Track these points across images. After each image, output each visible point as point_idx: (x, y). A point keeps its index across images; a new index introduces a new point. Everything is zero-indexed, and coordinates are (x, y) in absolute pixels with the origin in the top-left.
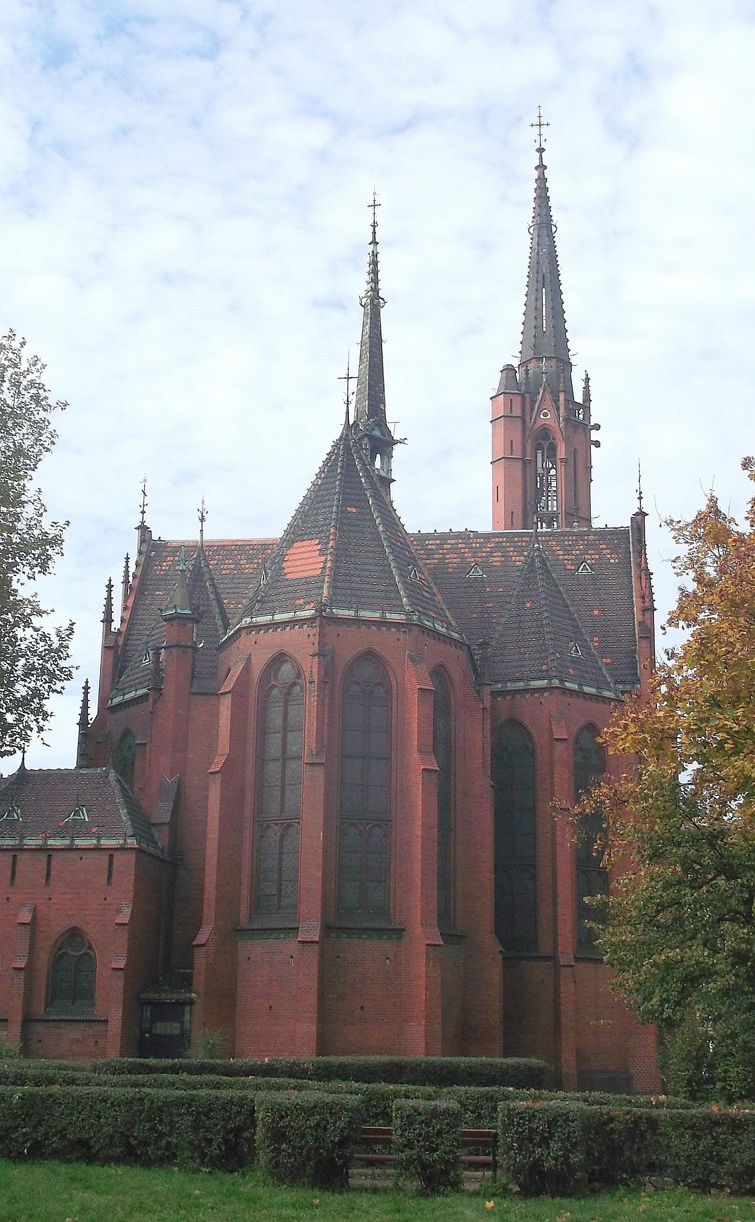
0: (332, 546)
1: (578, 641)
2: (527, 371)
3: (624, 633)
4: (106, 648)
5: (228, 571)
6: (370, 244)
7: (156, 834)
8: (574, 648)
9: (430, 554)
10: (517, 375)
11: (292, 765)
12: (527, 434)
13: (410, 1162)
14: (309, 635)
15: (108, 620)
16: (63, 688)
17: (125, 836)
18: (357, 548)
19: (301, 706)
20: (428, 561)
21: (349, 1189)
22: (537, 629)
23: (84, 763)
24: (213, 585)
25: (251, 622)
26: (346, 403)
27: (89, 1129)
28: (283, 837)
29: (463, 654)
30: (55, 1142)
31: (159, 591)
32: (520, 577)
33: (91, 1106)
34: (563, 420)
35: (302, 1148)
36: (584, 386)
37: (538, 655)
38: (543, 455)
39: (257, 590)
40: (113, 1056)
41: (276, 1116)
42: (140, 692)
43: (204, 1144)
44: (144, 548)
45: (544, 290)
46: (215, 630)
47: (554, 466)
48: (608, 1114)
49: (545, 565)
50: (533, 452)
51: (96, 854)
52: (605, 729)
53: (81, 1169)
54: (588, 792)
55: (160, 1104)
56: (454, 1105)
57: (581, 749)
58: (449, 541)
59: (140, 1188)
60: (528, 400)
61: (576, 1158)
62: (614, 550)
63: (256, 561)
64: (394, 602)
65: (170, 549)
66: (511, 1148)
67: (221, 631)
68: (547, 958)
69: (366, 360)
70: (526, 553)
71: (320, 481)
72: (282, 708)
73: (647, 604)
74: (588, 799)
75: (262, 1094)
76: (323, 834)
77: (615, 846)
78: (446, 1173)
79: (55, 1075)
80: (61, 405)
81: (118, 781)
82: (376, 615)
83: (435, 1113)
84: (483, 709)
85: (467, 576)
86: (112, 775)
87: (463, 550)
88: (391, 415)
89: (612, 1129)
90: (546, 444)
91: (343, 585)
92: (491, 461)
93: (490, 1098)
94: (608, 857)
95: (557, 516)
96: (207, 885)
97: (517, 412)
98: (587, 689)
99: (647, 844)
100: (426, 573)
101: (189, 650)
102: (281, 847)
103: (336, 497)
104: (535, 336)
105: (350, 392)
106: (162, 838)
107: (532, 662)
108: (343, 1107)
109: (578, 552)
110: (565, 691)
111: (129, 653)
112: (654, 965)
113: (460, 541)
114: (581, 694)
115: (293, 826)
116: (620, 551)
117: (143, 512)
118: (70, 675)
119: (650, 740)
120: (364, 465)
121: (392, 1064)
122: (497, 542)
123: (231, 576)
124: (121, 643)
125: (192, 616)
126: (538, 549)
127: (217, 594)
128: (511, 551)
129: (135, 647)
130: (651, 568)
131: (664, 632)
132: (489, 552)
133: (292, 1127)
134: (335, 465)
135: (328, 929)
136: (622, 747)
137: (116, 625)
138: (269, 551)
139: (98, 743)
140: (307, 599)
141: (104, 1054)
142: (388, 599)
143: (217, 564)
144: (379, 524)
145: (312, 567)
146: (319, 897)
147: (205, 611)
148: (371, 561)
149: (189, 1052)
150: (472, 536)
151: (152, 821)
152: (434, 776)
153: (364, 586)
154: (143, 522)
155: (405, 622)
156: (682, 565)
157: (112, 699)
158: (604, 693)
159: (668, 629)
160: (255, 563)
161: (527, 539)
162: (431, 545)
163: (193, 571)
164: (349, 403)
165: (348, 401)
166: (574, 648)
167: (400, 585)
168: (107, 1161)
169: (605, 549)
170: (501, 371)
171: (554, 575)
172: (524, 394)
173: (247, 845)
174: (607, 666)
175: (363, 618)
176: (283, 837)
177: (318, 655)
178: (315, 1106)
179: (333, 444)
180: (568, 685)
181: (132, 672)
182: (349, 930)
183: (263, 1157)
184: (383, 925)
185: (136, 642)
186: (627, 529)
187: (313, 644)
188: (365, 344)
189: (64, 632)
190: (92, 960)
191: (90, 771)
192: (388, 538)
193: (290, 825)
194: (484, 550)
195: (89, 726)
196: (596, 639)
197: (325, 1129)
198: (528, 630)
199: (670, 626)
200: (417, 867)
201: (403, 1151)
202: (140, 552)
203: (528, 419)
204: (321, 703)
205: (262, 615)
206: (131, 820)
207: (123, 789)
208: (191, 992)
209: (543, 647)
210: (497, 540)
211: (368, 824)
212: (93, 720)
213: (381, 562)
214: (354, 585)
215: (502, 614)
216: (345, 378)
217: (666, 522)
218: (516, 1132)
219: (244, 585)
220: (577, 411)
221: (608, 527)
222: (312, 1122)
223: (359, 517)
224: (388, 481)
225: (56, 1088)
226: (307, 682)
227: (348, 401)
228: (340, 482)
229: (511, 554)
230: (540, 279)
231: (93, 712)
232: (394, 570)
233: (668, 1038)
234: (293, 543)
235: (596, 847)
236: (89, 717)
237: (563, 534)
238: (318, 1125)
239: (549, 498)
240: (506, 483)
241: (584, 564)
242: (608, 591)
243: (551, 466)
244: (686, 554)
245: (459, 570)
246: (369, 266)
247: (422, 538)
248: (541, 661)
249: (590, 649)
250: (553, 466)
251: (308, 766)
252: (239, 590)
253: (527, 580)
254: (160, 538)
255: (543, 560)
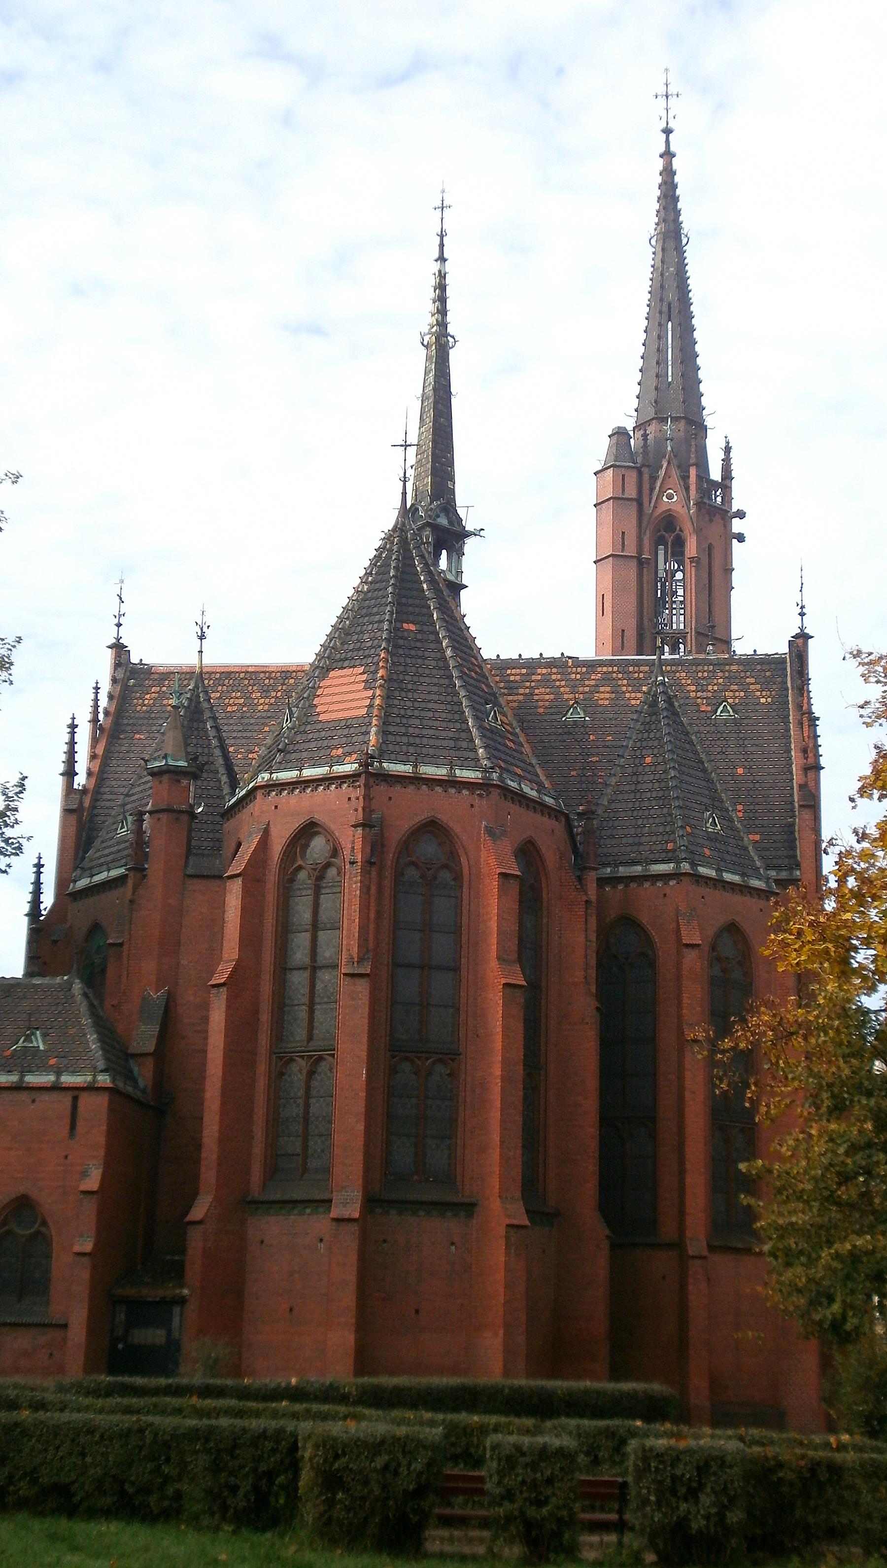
0: (382, 676)
1: (716, 811)
2: (645, 436)
3: (778, 799)
4: (67, 811)
5: (235, 708)
6: (436, 261)
7: (136, 1069)
8: (711, 820)
9: (512, 687)
10: (632, 441)
11: (324, 976)
12: (645, 523)
13: (509, 1519)
14: (349, 799)
15: (70, 773)
16: (9, 866)
17: (95, 1071)
18: (416, 679)
19: (338, 895)
20: (510, 698)
21: (427, 1556)
22: (661, 794)
23: (36, 969)
24: (217, 728)
25: (270, 779)
26: (403, 479)
27: (70, 1471)
28: (311, 1074)
29: (559, 827)
30: (24, 1489)
31: (138, 733)
32: (637, 721)
33: (73, 1441)
34: (694, 504)
35: (363, 1499)
36: (723, 457)
37: (661, 829)
38: (666, 553)
39: (278, 735)
40: (75, 1370)
41: (329, 1456)
42: (115, 873)
43: (226, 1494)
44: (120, 675)
45: (670, 324)
46: (218, 789)
47: (681, 568)
48: (775, 1458)
49: (671, 704)
50: (653, 545)
51: (55, 1096)
52: (773, 936)
53: (63, 1525)
54: (744, 1020)
55: (167, 1437)
56: (567, 1442)
57: (719, 959)
58: (539, 671)
59: (146, 1550)
60: (646, 477)
61: (735, 1517)
62: (766, 685)
63: (274, 694)
64: (466, 754)
65: (156, 676)
66: (645, 1502)
67: (226, 790)
68: (670, 1246)
69: (429, 421)
70: (644, 689)
71: (366, 587)
72: (311, 898)
73: (811, 760)
74: (743, 1029)
75: (305, 1426)
76: (367, 1071)
77: (777, 1094)
78: (557, 1535)
79: (17, 1396)
80: (11, 476)
81: (85, 995)
82: (441, 772)
83: (544, 1453)
84: (587, 902)
85: (563, 719)
86: (77, 987)
87: (558, 683)
88: (462, 498)
89: (779, 1479)
90: (670, 538)
91: (396, 729)
92: (595, 559)
93: (609, 1433)
94: (765, 1109)
95: (685, 637)
96: (205, 1140)
97: (631, 492)
98: (728, 877)
99: (826, 1091)
100: (510, 714)
101: (185, 818)
102: (308, 1089)
103: (388, 608)
104: (656, 389)
105: (408, 464)
106: (144, 1074)
107: (654, 839)
108: (421, 1445)
109: (716, 688)
110: (699, 879)
111: (99, 818)
112: (837, 1256)
113: (555, 670)
114: (718, 883)
115: (325, 1059)
116: (774, 687)
117: (119, 625)
118: (20, 848)
119: (835, 952)
120: (426, 565)
121: (464, 1388)
122: (605, 673)
123: (238, 715)
124: (86, 804)
125: (188, 769)
126: (663, 683)
127: (221, 740)
128: (624, 686)
129: (106, 811)
130: (817, 710)
131: (853, 804)
132: (593, 686)
133: (351, 1469)
134: (386, 565)
135: (371, 1202)
136: (796, 962)
137: (80, 780)
138: (292, 681)
139: (55, 942)
140: (347, 749)
141: (61, 1370)
142: (459, 749)
143: (220, 698)
144: (447, 647)
145: (355, 704)
146: (360, 1157)
147: (207, 763)
148: (436, 697)
149: (182, 1369)
150: (570, 664)
151: (131, 1050)
152: (518, 993)
153: (425, 732)
154: (118, 639)
155: (481, 781)
156: (873, 712)
157: (75, 881)
158: (752, 882)
159: (860, 801)
160: (273, 697)
161: (647, 669)
162: (514, 675)
163: (188, 707)
164: (407, 480)
165: (405, 477)
166: (711, 820)
167: (474, 731)
168: (92, 1514)
169: (752, 684)
170: (609, 436)
171: (684, 720)
172: (641, 467)
173: (261, 1084)
174: (757, 845)
175: (423, 776)
176: (311, 1074)
177: (364, 825)
178: (383, 1442)
179: (383, 535)
180: (702, 870)
181: (104, 845)
182: (391, 1203)
183: (309, 1512)
184: (451, 1198)
185: (108, 804)
186: (783, 656)
187: (356, 810)
188: (428, 398)
189: (11, 789)
190: (48, 1241)
191: (46, 980)
192: (458, 667)
193: (320, 1059)
194: (587, 683)
195: (41, 918)
196: (740, 807)
197: (396, 1473)
198: (649, 795)
199: (862, 796)
200: (495, 1115)
201: (500, 1505)
202: (114, 680)
203: (646, 500)
204: (365, 890)
205: (285, 769)
206: (103, 1049)
207: (91, 1006)
208: (182, 1286)
209: (669, 819)
210: (605, 669)
211: (427, 1059)
212: (47, 910)
213: (449, 698)
214: (411, 730)
215: (612, 772)
216: (402, 446)
217: (851, 653)
218: (654, 1481)
219: (256, 728)
220: (713, 492)
221: (758, 653)
222: (380, 1462)
223: (419, 637)
224: (457, 588)
225: (25, 1414)
226: (347, 864)
227: (405, 477)
228: (394, 589)
229: (624, 689)
230: (665, 309)
231: (48, 900)
232: (467, 710)
233: (838, 1358)
234: (328, 670)
235: (749, 1095)
236: (42, 906)
237: (696, 663)
238: (386, 1467)
239: (674, 612)
240: (614, 589)
241: (724, 704)
242: (756, 742)
243: (676, 567)
244: (879, 697)
245: (553, 710)
246: (435, 291)
247: (502, 665)
248: (666, 838)
249: (732, 821)
250: (679, 567)
251: (348, 979)
252: (249, 734)
253: (647, 726)
254: (141, 660)
255: (669, 698)
